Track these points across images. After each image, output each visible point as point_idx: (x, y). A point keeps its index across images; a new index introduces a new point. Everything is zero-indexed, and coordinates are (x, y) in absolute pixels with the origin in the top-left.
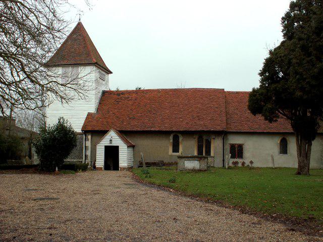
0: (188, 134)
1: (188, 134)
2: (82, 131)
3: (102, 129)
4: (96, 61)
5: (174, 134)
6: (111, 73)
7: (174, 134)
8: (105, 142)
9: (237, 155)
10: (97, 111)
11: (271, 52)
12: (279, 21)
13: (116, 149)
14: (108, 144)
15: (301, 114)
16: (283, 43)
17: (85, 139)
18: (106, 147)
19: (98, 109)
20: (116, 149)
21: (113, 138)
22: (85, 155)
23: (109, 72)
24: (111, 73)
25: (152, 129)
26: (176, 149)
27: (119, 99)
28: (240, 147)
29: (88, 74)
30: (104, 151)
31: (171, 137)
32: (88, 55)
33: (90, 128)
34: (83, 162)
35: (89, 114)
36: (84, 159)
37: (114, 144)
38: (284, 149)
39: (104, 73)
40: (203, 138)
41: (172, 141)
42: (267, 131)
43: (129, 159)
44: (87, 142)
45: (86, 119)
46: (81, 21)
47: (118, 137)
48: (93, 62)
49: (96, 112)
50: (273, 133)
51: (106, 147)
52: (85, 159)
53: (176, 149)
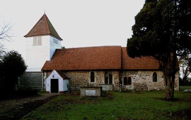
1: (98, 70)
2: (42, 71)
5: (91, 71)
6: (62, 40)
7: (91, 71)
8: (51, 77)
12: (131, 28)
15: (166, 56)
16: (131, 38)
18: (51, 79)
19: (52, 59)
21: (55, 75)
22: (44, 84)
23: (61, 39)
24: (62, 40)
26: (92, 80)
27: (63, 53)
28: (130, 79)
29: (47, 39)
30: (50, 82)
31: (90, 73)
33: (45, 69)
36: (43, 86)
37: (55, 78)
38: (155, 79)
40: (108, 72)
41: (90, 75)
42: (145, 69)
43: (64, 87)
44: (44, 77)
50: (96, 70)
51: (51, 79)
52: (44, 86)
53: (92, 80)
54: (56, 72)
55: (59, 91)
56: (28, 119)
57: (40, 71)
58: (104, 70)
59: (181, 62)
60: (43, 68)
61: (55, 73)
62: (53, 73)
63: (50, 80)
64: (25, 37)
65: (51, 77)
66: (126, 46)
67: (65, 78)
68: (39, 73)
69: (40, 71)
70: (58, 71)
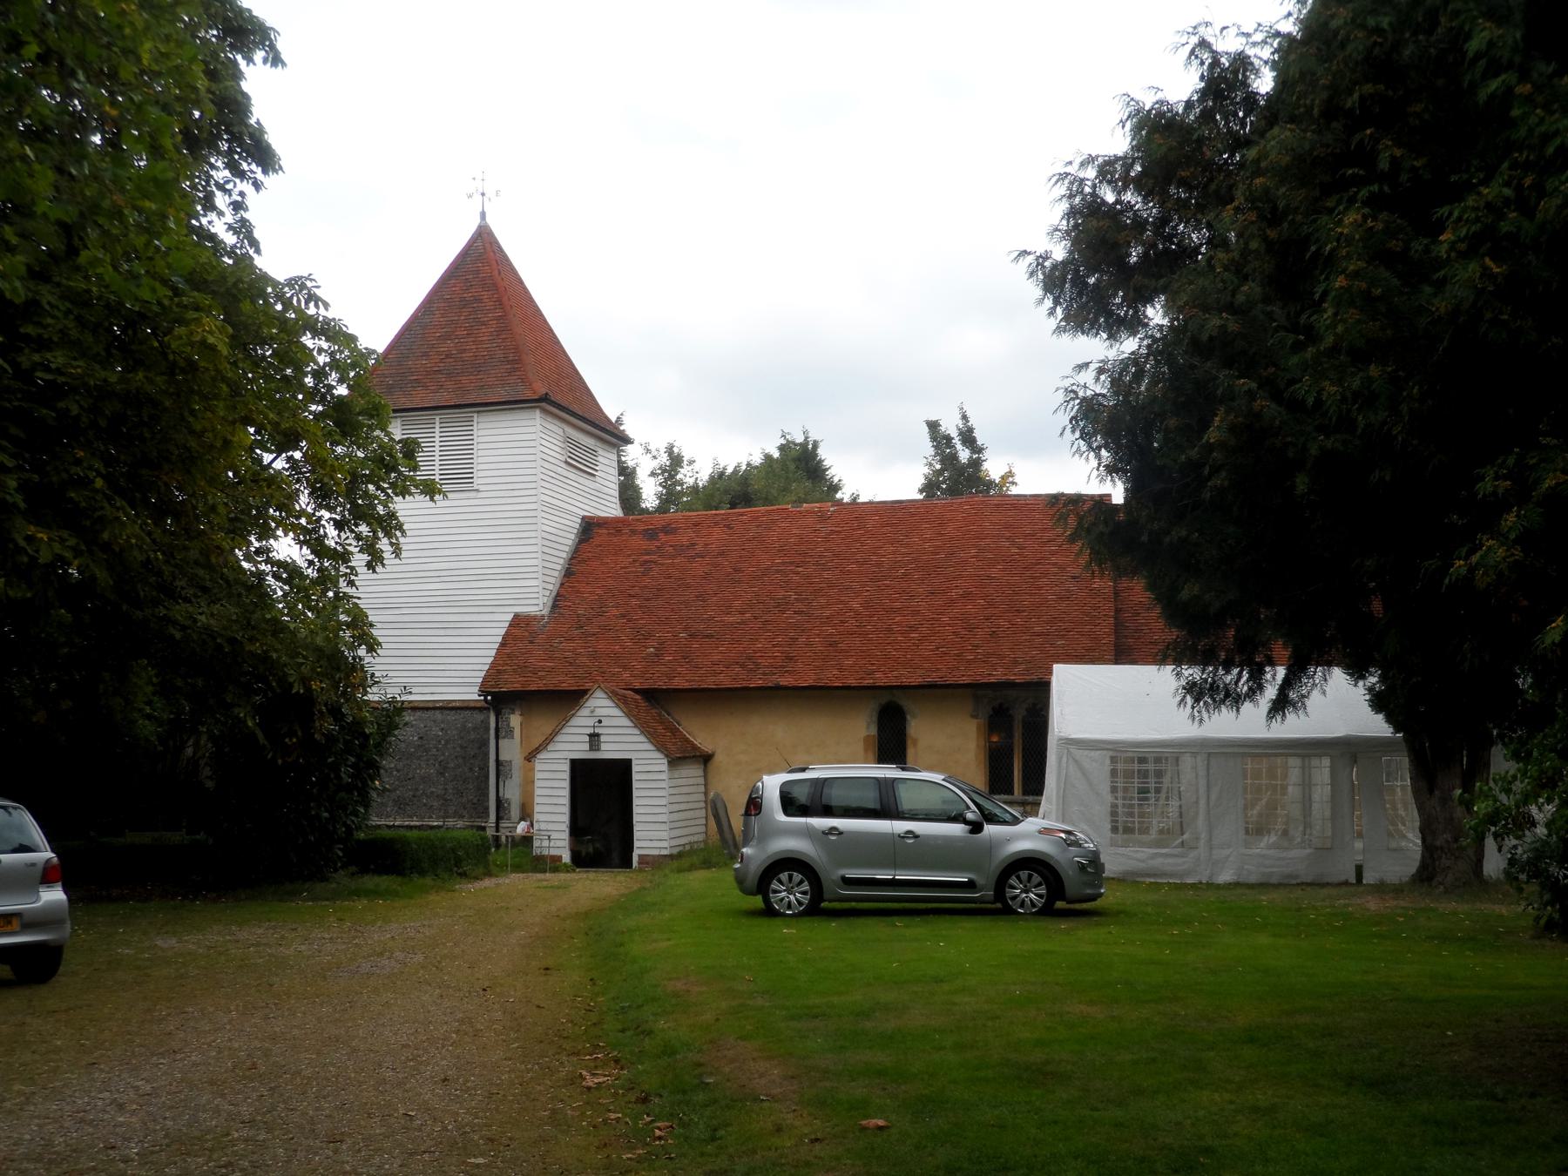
0: (938, 693)
1: (938, 693)
3: (568, 684)
4: (543, 391)
8: (571, 744)
9: (1136, 773)
10: (555, 606)
11: (298, 283)
13: (620, 772)
14: (581, 751)
17: (497, 730)
18: (574, 763)
19: (558, 601)
20: (620, 772)
25: (784, 681)
30: (635, 793)
32: (515, 363)
33: (512, 683)
34: (490, 832)
35: (518, 621)
36: (493, 817)
37: (611, 750)
39: (589, 442)
45: (503, 645)
46: (490, 221)
47: (626, 722)
48: (529, 395)
49: (546, 612)
51: (574, 763)
52: (498, 818)
54: (608, 703)
55: (806, 882)
56: (2, 462)
57: (472, 694)
58: (976, 691)
59: (1203, 671)
60: (494, 672)
61: (599, 712)
62: (584, 712)
63: (566, 767)
64: (263, 252)
65: (571, 744)
66: (1113, 503)
67: (684, 755)
68: (451, 716)
69: (472, 694)
70: (621, 700)
